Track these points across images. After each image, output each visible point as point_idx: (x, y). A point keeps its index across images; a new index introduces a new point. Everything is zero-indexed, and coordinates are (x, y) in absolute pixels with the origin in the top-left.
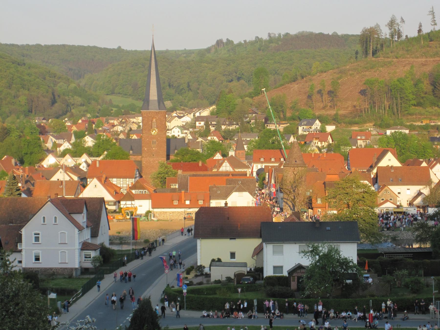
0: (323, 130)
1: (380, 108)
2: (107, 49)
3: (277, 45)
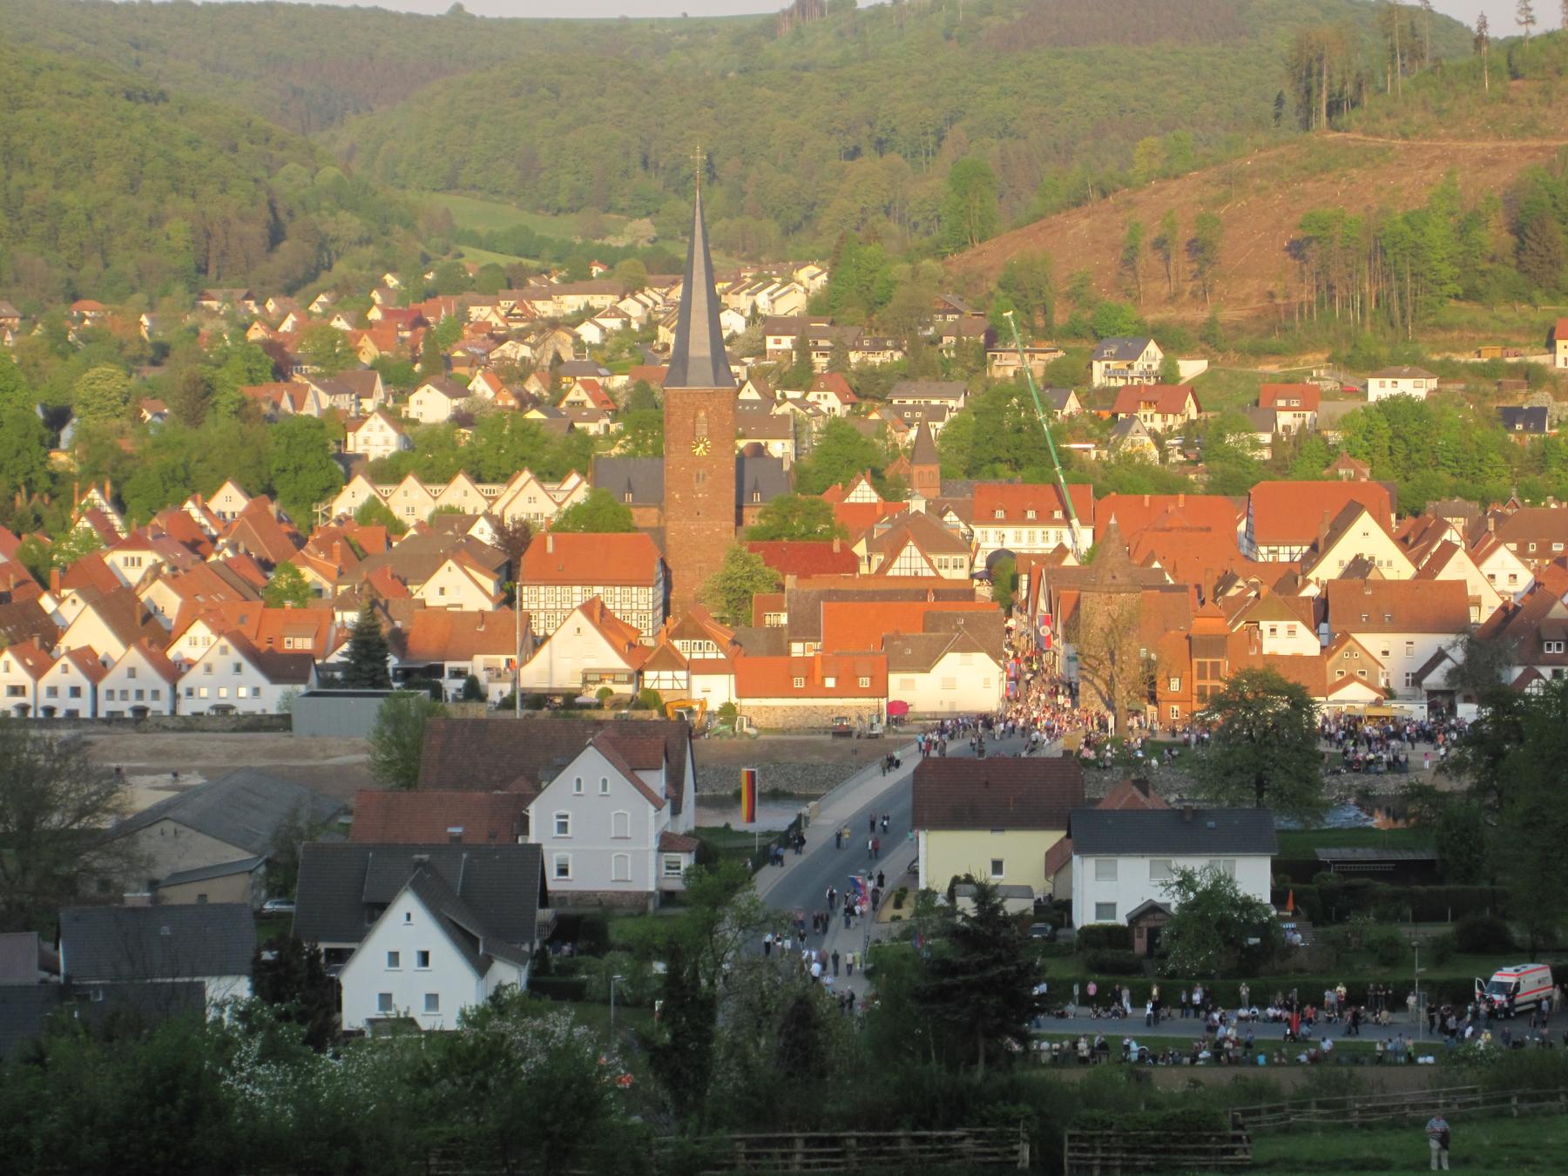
0: (1168, 376)
1: (1346, 303)
2: (419, 16)
3: (1006, 22)
